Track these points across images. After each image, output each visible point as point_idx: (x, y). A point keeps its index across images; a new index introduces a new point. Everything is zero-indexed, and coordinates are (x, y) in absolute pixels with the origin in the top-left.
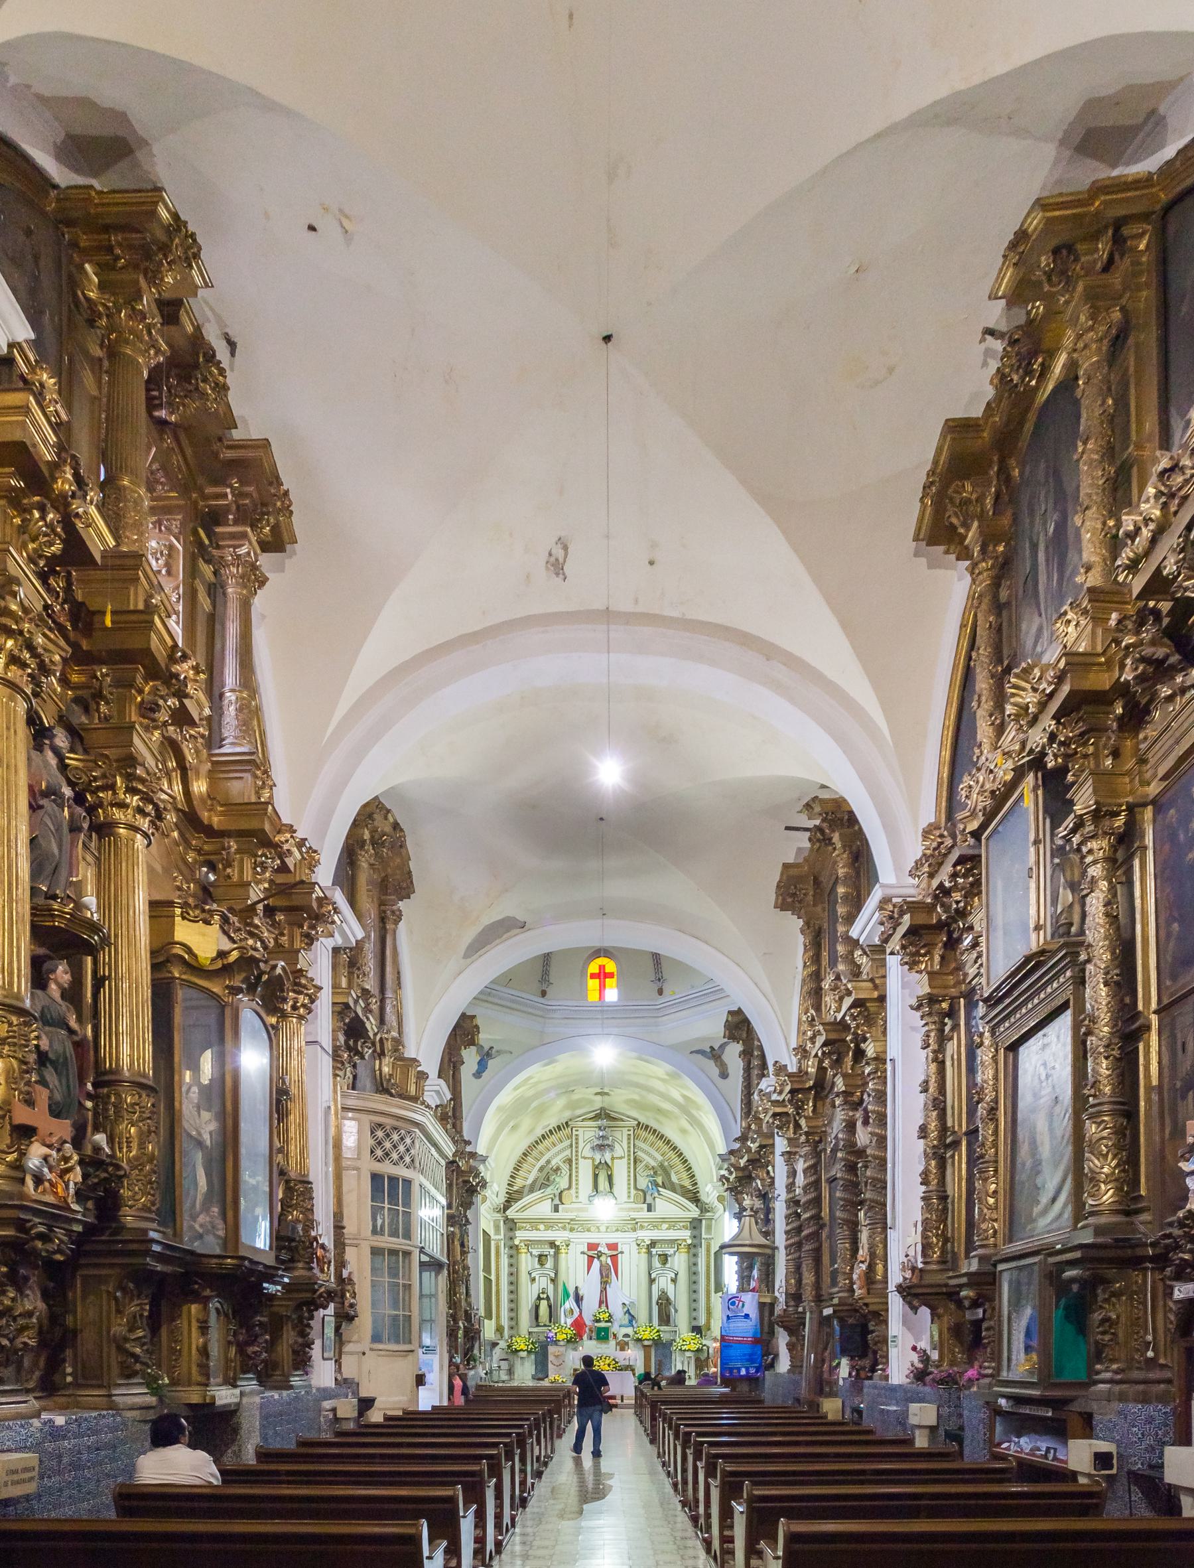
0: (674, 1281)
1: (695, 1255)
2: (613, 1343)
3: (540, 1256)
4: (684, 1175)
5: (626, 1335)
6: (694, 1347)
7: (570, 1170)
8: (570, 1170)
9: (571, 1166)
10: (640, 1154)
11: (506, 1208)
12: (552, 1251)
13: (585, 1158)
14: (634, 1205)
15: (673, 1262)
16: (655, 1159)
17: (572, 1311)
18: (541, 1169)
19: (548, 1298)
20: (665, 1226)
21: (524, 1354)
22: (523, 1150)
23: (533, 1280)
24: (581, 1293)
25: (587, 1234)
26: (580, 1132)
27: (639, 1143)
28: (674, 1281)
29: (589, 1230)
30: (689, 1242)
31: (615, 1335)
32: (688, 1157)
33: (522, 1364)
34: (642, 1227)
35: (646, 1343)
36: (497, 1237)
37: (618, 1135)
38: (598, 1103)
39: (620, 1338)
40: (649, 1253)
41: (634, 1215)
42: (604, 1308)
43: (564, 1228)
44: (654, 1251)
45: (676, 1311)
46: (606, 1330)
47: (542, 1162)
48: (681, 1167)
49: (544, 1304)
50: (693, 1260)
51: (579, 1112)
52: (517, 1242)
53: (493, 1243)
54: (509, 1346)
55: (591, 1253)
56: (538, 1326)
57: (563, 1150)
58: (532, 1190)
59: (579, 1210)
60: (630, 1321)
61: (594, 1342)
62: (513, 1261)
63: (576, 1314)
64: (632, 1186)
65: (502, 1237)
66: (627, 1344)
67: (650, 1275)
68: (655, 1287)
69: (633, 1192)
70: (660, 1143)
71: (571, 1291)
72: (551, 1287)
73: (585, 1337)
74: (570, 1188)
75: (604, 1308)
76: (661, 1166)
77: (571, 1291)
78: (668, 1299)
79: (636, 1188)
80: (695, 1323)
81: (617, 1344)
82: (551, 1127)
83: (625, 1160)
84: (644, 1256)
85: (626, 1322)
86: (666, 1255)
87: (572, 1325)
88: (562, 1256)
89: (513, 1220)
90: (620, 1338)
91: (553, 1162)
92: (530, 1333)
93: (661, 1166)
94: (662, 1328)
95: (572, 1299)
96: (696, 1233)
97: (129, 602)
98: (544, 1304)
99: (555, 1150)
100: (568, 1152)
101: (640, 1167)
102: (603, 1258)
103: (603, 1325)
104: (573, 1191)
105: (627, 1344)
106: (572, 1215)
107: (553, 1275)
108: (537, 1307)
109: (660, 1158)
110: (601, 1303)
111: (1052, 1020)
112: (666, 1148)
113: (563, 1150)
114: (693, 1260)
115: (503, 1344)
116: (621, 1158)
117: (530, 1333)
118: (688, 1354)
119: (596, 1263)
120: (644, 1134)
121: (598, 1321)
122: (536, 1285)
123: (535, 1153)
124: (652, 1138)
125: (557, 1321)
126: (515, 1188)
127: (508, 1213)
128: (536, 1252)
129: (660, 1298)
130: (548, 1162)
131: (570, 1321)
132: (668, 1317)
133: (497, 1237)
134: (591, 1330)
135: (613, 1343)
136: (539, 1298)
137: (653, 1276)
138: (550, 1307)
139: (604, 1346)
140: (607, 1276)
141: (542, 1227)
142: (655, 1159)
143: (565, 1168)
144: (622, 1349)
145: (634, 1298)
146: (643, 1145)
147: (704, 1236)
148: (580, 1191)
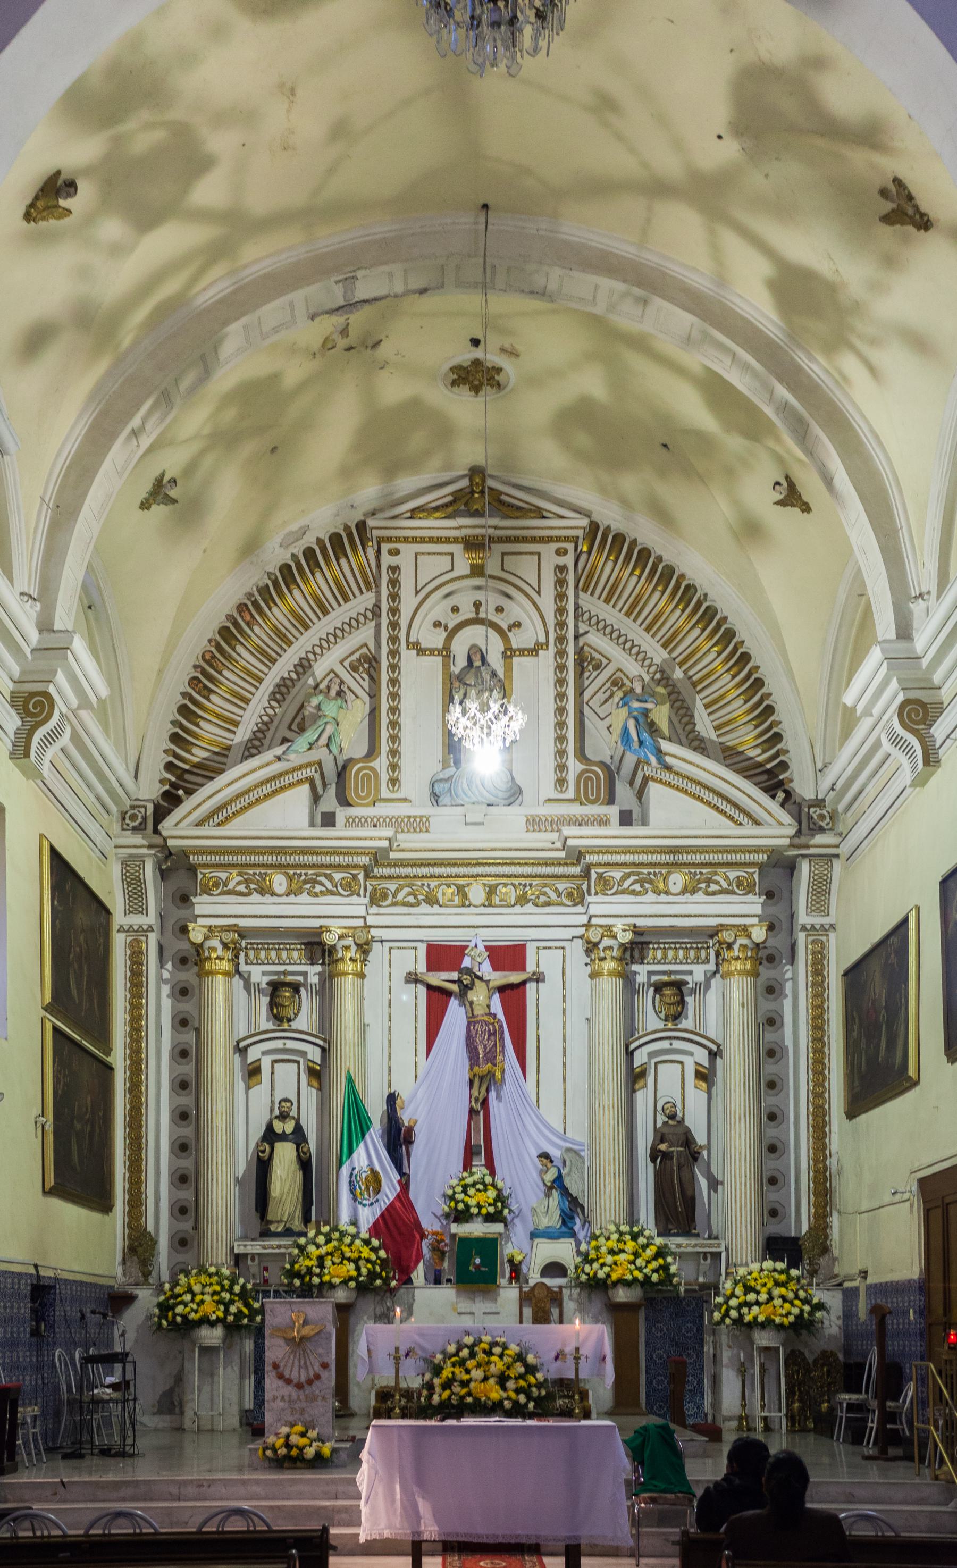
0: (705, 1076)
1: (772, 990)
2: (509, 1294)
3: (276, 987)
4: (738, 708)
5: (554, 1269)
6: (785, 1313)
7: (374, 695)
8: (374, 695)
9: (374, 680)
10: (595, 639)
11: (160, 814)
12: (313, 973)
13: (421, 651)
14: (576, 810)
15: (701, 1016)
16: (641, 657)
17: (375, 1181)
18: (281, 691)
19: (299, 1136)
20: (677, 880)
21: (213, 1336)
22: (219, 620)
23: (253, 1072)
24: (405, 1117)
25: (426, 915)
26: (405, 559)
27: (592, 604)
28: (705, 1076)
29: (431, 900)
30: (759, 934)
31: (516, 1272)
32: (750, 646)
33: (209, 1374)
34: (605, 884)
35: (622, 1295)
36: (137, 920)
37: (525, 568)
38: (467, 355)
39: (535, 1277)
40: (628, 979)
41: (580, 837)
42: (479, 1171)
43: (350, 888)
44: (641, 972)
45: (714, 1184)
46: (488, 1247)
47: (285, 665)
48: (725, 683)
49: (285, 1154)
50: (768, 1005)
51: (406, 483)
52: (197, 935)
53: (119, 945)
54: (165, 1308)
55: (438, 979)
56: (266, 1234)
57: (352, 625)
58: (252, 748)
59: (401, 824)
60: (567, 1218)
61: (446, 1293)
62: (187, 1007)
63: (389, 1192)
64: (571, 748)
65: (151, 919)
66: (556, 1298)
67: (630, 1054)
68: (643, 1099)
69: (574, 766)
70: (658, 601)
71: (376, 1110)
72: (310, 1096)
73: (419, 1274)
74: (372, 751)
75: (479, 1171)
76: (664, 679)
77: (376, 1110)
78: (687, 1140)
79: (581, 754)
80: (774, 1229)
81: (525, 1299)
82: (310, 540)
83: (548, 657)
84: (609, 987)
85: (552, 1220)
86: (679, 986)
87: (375, 1230)
88: (347, 985)
89: (184, 853)
90: (535, 1277)
91: (320, 669)
92: (238, 1259)
93: (664, 679)
94: (675, 1242)
95: (375, 1133)
96: (778, 910)
97: (647, 1526)
98: (285, 1154)
99: (322, 627)
100: (365, 634)
101: (596, 682)
102: (478, 995)
103: (476, 1229)
104: (381, 763)
105: (556, 1298)
106: (376, 838)
107: (314, 1054)
108: (263, 1167)
109: (659, 655)
110: (470, 1153)
111: (623, 1130)
112: (677, 618)
113: (352, 625)
114: (768, 1005)
115: (146, 1299)
116: (533, 651)
117: (238, 1259)
118: (763, 1339)
119: (455, 1014)
120: (608, 570)
121: (462, 1216)
122: (261, 1093)
123: (259, 633)
124: (633, 583)
125: (329, 1216)
126: (199, 755)
127: (167, 826)
128: (259, 974)
129: (661, 1137)
130: (304, 666)
131: (368, 1216)
132: (690, 1202)
133: (137, 920)
134: (437, 1249)
135: (509, 1294)
136: (270, 1136)
137: (640, 1058)
138: (304, 1164)
139: (480, 1306)
140: (491, 1057)
141: (279, 881)
142: (641, 657)
143: (357, 684)
144: (541, 1317)
145: (578, 1134)
146: (612, 615)
147: (803, 918)
148: (405, 762)
